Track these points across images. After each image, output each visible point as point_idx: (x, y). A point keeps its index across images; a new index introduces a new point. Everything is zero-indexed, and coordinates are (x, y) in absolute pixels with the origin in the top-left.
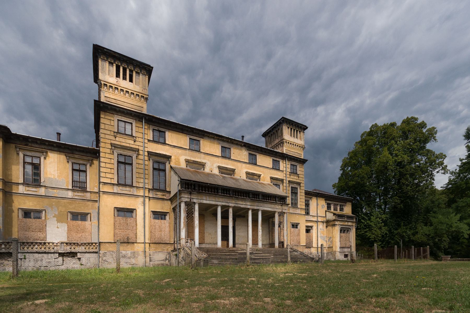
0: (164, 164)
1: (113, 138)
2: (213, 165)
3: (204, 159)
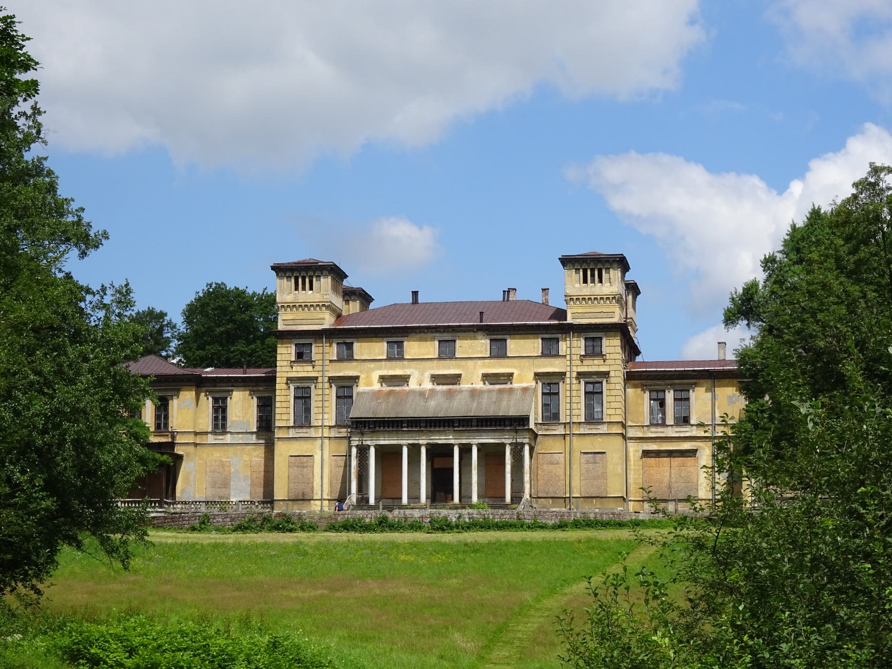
0: (351, 387)
2: (423, 374)
3: (409, 367)
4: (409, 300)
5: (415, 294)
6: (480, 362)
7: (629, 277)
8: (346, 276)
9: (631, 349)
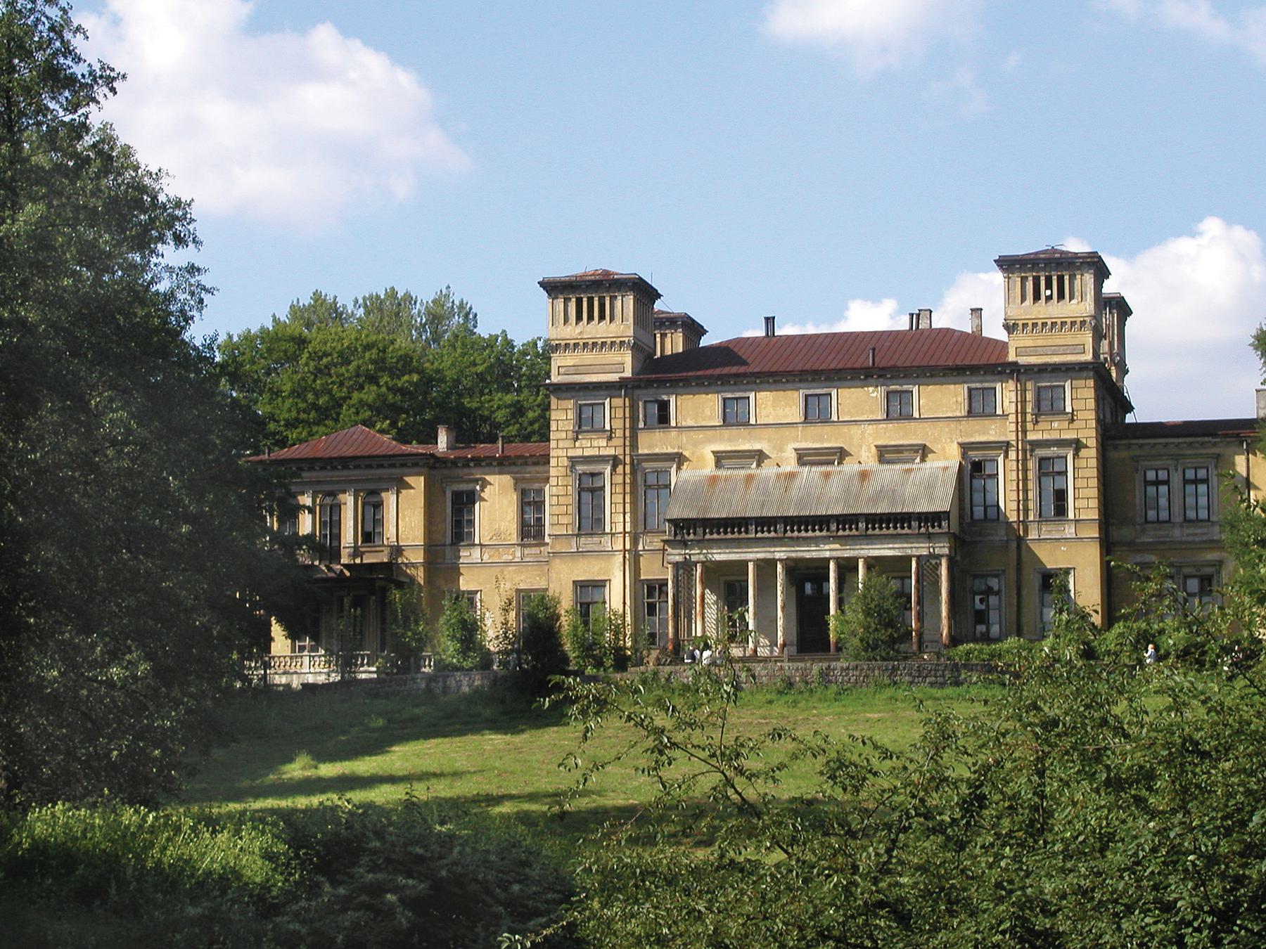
6: (870, 429)
7: (1109, 287)
8: (659, 296)
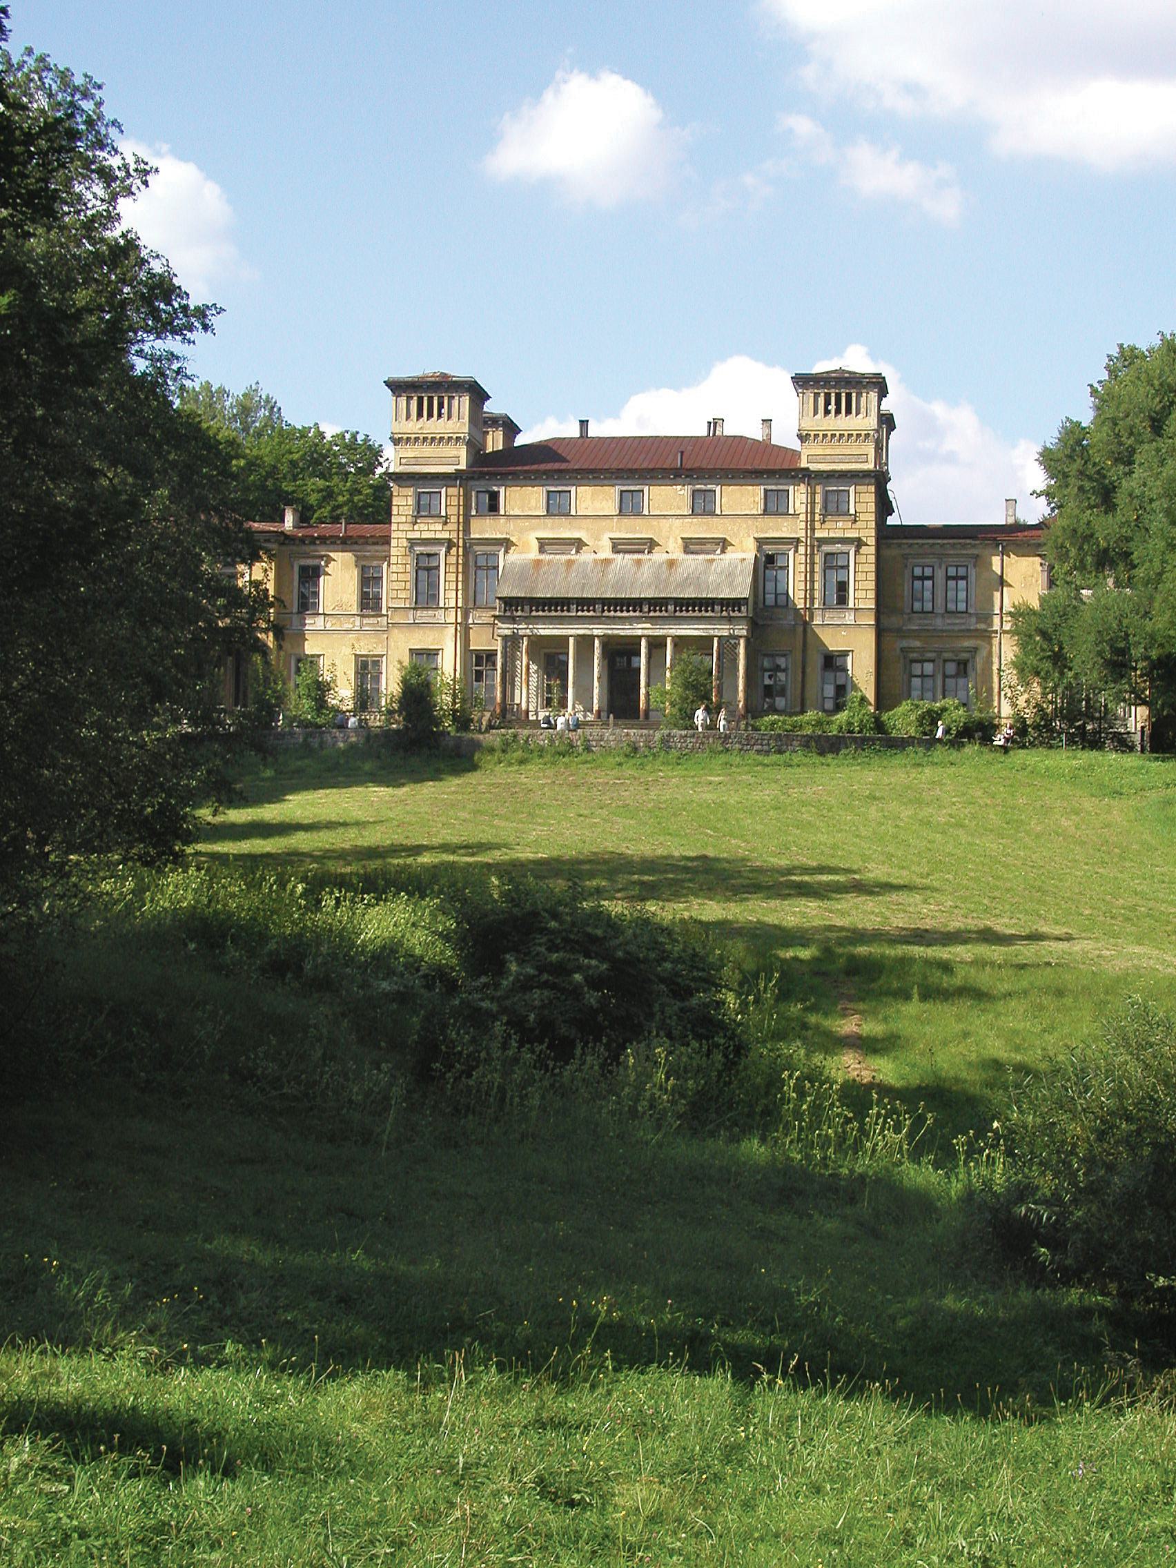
1: (408, 527)
4: (574, 432)
5: (584, 424)
6: (678, 522)
7: (887, 405)
9: (884, 506)
